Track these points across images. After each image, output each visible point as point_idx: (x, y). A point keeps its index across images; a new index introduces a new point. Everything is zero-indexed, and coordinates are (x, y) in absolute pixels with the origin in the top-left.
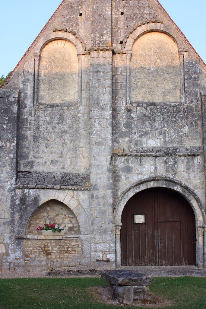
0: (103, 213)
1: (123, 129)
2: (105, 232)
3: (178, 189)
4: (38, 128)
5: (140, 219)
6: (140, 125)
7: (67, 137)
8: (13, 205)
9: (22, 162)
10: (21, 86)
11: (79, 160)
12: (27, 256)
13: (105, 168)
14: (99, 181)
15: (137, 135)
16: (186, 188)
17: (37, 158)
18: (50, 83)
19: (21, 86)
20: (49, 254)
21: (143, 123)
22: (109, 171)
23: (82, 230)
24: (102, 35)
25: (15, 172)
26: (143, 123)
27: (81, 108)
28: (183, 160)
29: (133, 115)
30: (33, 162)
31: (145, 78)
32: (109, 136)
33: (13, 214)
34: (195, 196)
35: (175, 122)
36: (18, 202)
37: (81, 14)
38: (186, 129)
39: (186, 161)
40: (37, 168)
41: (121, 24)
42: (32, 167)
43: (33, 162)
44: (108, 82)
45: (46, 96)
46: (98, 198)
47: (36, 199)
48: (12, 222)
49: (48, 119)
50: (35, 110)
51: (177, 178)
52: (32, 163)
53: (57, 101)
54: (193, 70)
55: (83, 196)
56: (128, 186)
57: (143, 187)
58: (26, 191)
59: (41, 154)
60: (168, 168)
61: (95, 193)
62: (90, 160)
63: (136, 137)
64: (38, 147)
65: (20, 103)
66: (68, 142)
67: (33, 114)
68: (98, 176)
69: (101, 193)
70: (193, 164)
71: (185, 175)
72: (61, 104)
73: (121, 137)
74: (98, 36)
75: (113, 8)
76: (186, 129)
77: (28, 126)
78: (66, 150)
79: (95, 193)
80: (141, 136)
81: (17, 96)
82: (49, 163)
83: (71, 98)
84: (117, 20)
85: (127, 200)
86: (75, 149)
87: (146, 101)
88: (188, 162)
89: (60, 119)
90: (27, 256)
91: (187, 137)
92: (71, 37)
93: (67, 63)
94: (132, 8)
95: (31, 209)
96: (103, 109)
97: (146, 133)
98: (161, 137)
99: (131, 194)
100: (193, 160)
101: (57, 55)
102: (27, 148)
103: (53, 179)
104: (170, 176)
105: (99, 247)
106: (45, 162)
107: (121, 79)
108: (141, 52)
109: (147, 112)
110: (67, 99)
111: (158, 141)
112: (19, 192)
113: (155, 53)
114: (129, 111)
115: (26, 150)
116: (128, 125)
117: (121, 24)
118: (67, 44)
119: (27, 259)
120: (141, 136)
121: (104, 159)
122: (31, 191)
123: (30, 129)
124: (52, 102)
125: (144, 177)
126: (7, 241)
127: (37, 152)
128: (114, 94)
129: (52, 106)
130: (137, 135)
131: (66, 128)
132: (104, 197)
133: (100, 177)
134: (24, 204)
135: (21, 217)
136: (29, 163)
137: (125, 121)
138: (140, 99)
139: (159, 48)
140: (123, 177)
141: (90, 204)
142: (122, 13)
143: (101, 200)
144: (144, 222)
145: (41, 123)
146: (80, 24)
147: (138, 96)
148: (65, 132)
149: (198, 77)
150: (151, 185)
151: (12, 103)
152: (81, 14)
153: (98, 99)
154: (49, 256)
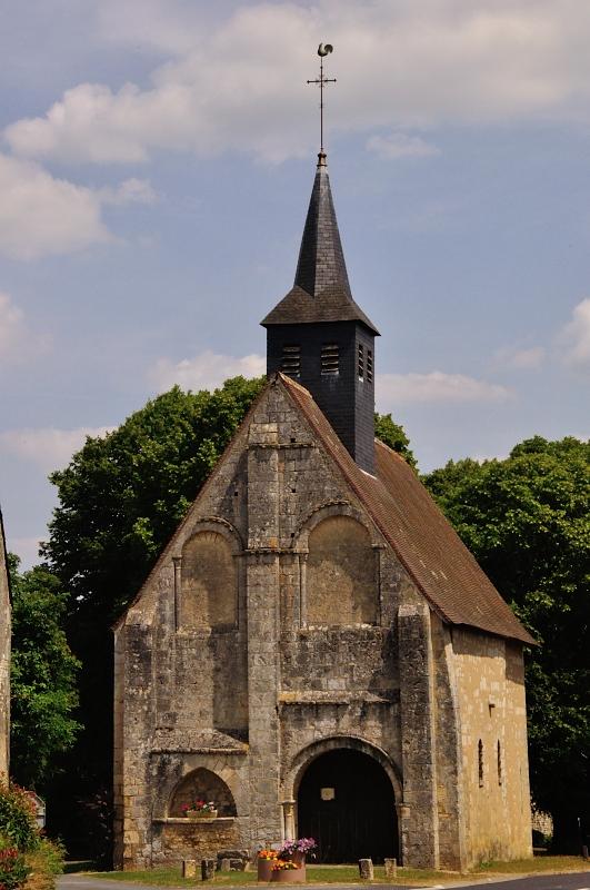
1: (295, 664)
5: (328, 794)
11: (237, 711)
12: (168, 847)
14: (259, 741)
17: (181, 708)
20: (197, 843)
21: (322, 656)
23: (239, 810)
25: (318, 246)
26: (322, 656)
28: (374, 710)
29: (308, 644)
30: (175, 714)
33: (148, 790)
35: (366, 653)
36: (155, 773)
37: (236, 494)
39: (378, 711)
43: (175, 714)
49: (194, 651)
57: (320, 749)
60: (353, 721)
64: (182, 692)
66: (222, 685)
67: (174, 645)
68: (259, 735)
70: (389, 716)
74: (258, 530)
75: (297, 451)
77: (169, 662)
78: (219, 695)
80: (319, 675)
82: (197, 715)
83: (227, 618)
93: (219, 567)
94: (308, 482)
95: (172, 782)
97: (326, 670)
98: (347, 675)
100: (388, 709)
101: (206, 555)
102: (168, 694)
103: (201, 740)
106: (192, 714)
108: (321, 548)
111: (343, 681)
113: (342, 548)
116: (302, 659)
119: (168, 851)
120: (319, 675)
127: (181, 700)
134: (163, 775)
135: (160, 791)
137: (298, 652)
139: (346, 540)
142: (294, 491)
145: (185, 658)
146: (235, 509)
149: (399, 586)
150: (332, 745)
152: (236, 494)
153: (257, 625)
154: (196, 847)
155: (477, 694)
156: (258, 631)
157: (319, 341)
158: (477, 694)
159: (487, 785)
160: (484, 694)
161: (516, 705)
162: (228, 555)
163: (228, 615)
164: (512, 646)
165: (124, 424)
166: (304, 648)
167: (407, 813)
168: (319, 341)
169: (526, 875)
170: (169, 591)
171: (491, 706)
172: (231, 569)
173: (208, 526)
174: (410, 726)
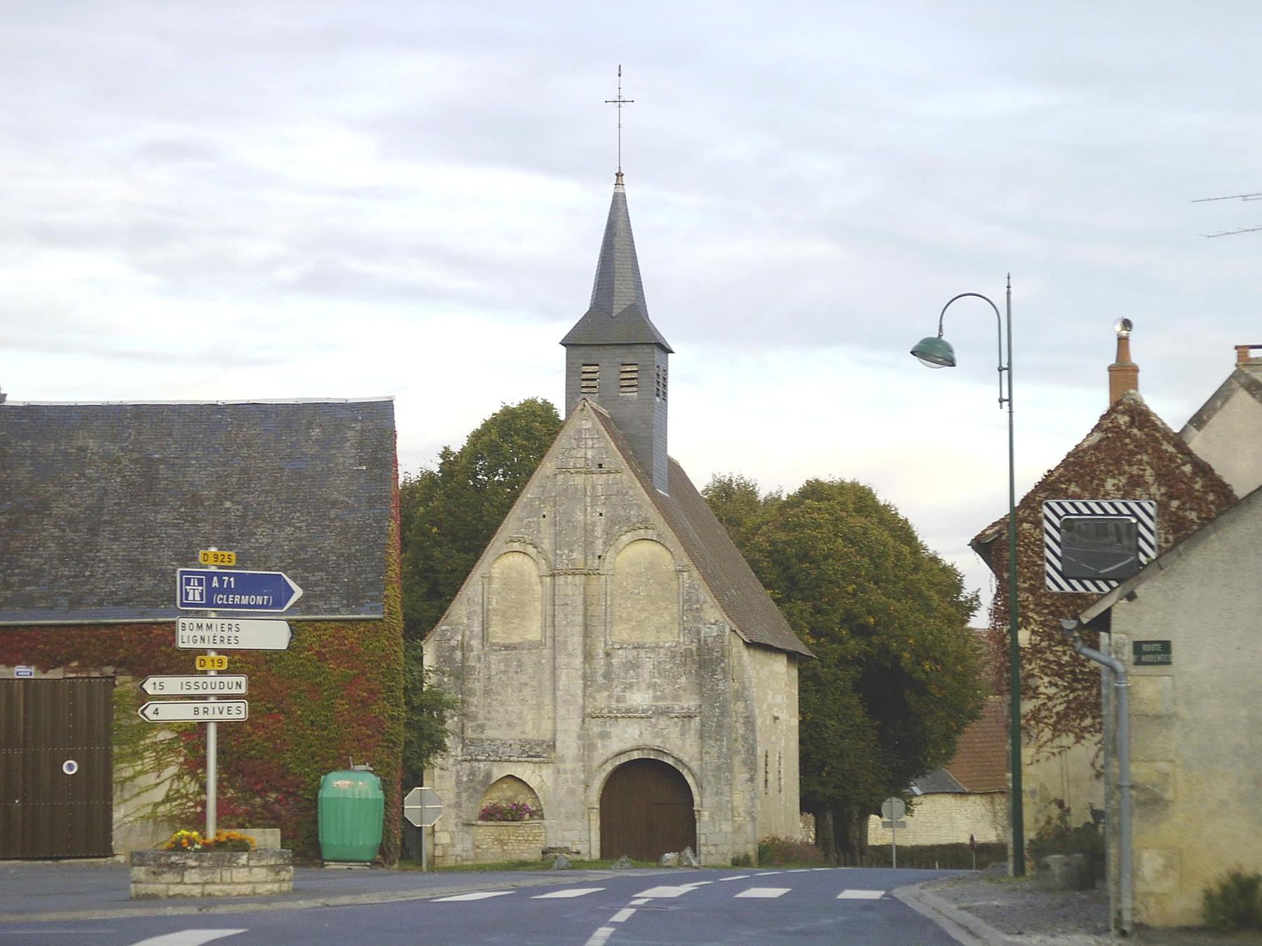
0: (571, 792)
1: (601, 680)
2: (574, 815)
3: (670, 761)
4: (489, 678)
5: (70, 768)
6: (622, 674)
7: (527, 692)
8: (459, 783)
9: (469, 724)
10: (465, 621)
13: (574, 735)
15: (619, 689)
16: (677, 760)
18: (504, 615)
19: (465, 621)
21: (627, 672)
22: (579, 737)
24: (571, 551)
27: (545, 652)
31: (633, 607)
32: (579, 692)
33: (458, 795)
34: (689, 770)
38: (683, 679)
40: (490, 733)
41: (599, 531)
42: (482, 732)
44: (580, 619)
45: (498, 633)
46: (565, 772)
47: (488, 775)
48: (458, 805)
49: (502, 667)
50: (486, 655)
51: (668, 747)
52: (481, 728)
53: (515, 639)
54: (694, 598)
55: (547, 771)
56: (603, 759)
57: (624, 759)
58: (476, 764)
59: (493, 715)
61: (562, 766)
62: (555, 723)
63: (617, 691)
65: (464, 647)
69: (569, 765)
71: (679, 742)
72: (519, 644)
73: (598, 691)
76: (683, 679)
79: (562, 766)
81: (460, 638)
84: (594, 524)
85: (604, 775)
86: (539, 707)
87: (633, 640)
88: (683, 725)
89: (519, 666)
90: (478, 847)
91: (685, 690)
92: (530, 550)
96: (570, 655)
99: (609, 768)
101: (514, 575)
104: (657, 742)
105: (567, 834)
107: (598, 611)
109: (631, 654)
110: (529, 637)
112: (466, 765)
114: (608, 655)
115: (473, 708)
116: (607, 676)
117: (599, 531)
118: (526, 559)
120: (624, 690)
121: (574, 724)
122: (482, 765)
123: (478, 680)
124: (507, 641)
125: (628, 746)
126: (452, 828)
127: (489, 712)
128: (587, 633)
129: (507, 648)
130: (619, 689)
131: (525, 679)
132: (573, 771)
133: (568, 745)
136: (478, 726)
138: (625, 636)
140: (599, 745)
141: (556, 782)
143: (569, 776)
144: (278, 831)
147: (621, 633)
148: (526, 684)
150: (636, 755)
151: (453, 649)
155: (765, 707)
156: (565, 648)
157: (617, 341)
158: (765, 707)
159: (771, 792)
160: (770, 707)
161: (791, 716)
162: (535, 574)
163: (588, 641)
164: (792, 657)
165: (456, 449)
166: (610, 665)
167: (706, 816)
168: (617, 341)
169: (364, 899)
170: (478, 609)
171: (776, 718)
172: (538, 588)
173: (516, 546)
174: (710, 738)
